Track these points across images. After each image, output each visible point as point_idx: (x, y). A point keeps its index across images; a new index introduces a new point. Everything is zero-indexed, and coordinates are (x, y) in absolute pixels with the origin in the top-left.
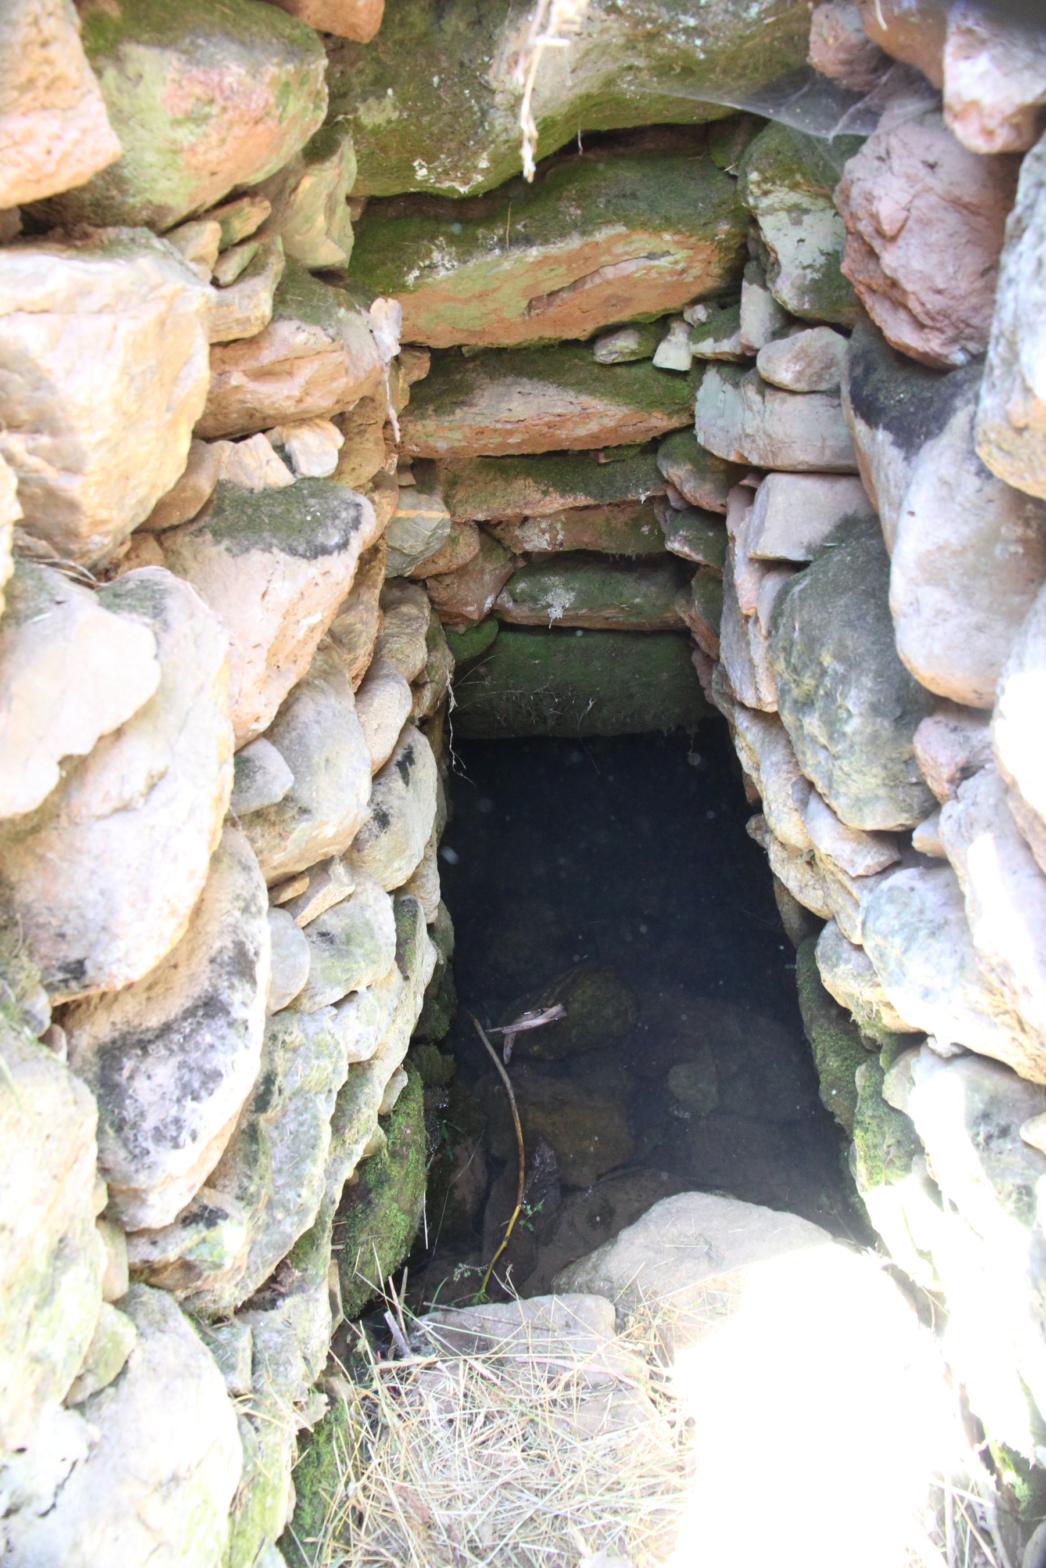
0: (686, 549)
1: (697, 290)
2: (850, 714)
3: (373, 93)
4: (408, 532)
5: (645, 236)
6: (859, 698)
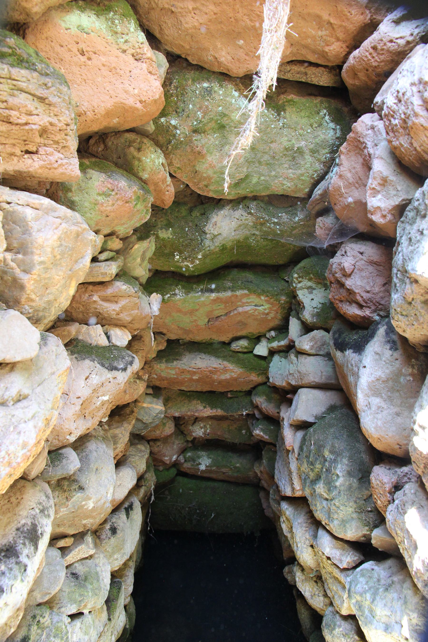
0: (262, 433)
1: (272, 324)
2: (338, 476)
3: (165, 228)
4: (146, 413)
5: (255, 297)
6: (342, 468)
